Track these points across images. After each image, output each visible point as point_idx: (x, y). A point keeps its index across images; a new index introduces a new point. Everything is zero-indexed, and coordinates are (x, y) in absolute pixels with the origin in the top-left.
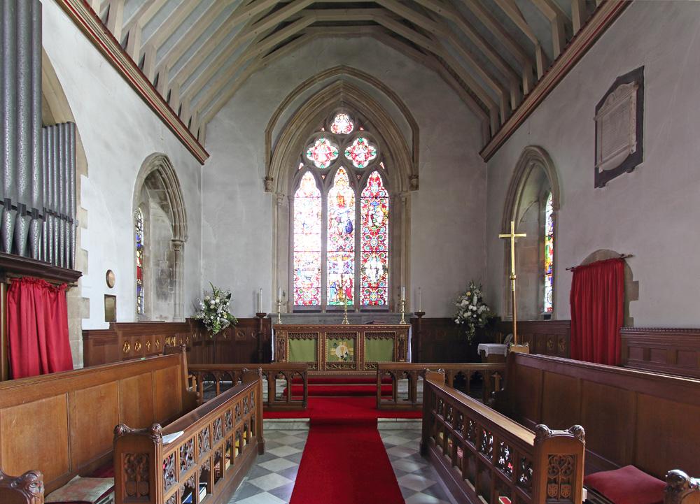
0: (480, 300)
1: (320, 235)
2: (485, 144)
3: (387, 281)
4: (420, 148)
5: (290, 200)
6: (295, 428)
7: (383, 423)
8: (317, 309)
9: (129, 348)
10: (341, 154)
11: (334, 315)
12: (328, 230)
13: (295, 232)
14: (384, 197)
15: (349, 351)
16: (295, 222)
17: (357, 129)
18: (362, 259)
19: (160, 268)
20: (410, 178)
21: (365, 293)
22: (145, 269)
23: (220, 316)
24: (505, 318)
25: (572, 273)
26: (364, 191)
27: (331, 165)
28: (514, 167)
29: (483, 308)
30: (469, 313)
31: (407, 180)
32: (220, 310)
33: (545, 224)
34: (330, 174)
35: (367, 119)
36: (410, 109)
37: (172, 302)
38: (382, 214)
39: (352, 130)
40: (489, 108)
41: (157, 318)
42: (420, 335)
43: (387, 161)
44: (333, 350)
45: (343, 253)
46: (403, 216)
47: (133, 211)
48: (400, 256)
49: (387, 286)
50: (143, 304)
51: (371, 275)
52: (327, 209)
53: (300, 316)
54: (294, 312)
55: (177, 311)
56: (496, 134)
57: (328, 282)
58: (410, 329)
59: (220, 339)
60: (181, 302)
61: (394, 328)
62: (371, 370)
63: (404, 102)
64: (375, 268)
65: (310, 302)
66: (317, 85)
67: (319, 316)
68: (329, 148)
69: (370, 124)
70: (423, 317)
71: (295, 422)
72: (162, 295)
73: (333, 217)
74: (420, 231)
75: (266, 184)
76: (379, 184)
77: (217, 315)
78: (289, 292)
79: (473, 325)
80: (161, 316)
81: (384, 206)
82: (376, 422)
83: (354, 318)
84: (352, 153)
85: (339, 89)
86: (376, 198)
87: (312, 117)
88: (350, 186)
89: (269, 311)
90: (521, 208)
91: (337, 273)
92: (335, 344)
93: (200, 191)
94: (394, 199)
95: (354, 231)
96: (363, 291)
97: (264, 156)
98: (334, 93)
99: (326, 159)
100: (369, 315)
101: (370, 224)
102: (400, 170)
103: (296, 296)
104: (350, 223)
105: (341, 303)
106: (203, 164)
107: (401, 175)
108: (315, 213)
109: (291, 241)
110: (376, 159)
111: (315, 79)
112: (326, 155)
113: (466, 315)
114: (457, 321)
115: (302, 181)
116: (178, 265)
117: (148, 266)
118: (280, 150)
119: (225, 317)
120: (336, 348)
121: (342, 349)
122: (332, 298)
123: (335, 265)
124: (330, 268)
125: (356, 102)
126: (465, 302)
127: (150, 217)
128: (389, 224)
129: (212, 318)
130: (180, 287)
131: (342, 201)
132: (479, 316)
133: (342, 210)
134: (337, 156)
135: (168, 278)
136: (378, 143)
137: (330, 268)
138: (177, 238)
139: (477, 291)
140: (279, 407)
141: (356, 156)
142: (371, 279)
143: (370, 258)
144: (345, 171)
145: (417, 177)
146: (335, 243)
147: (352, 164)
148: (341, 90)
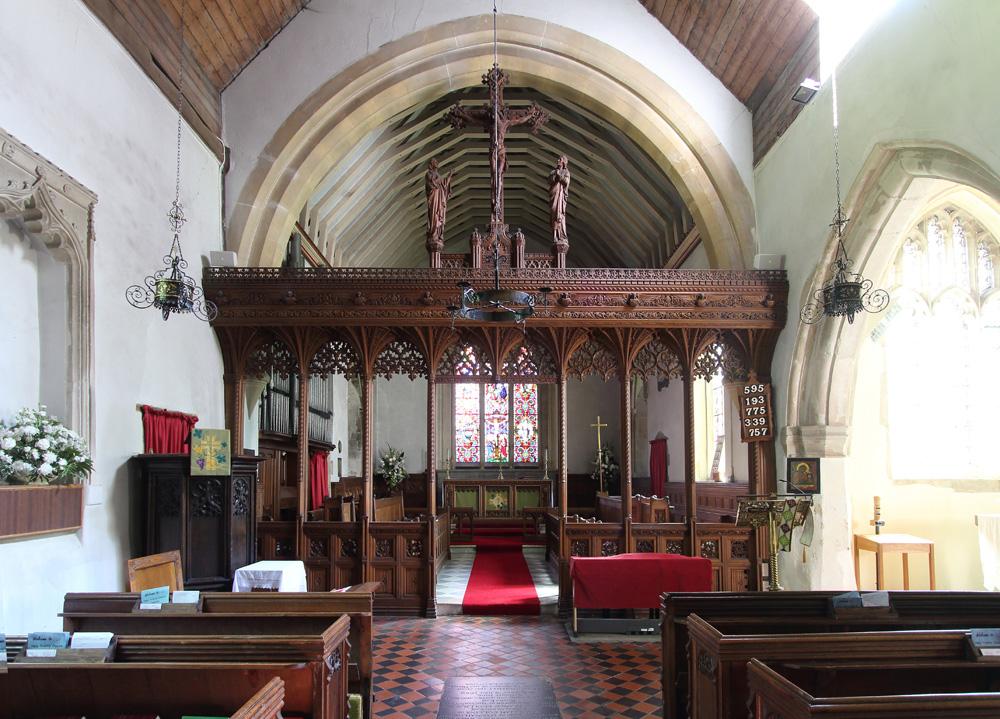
64: (527, 429)
65: (471, 459)
122: (490, 456)
123: (491, 426)
132: (611, 473)
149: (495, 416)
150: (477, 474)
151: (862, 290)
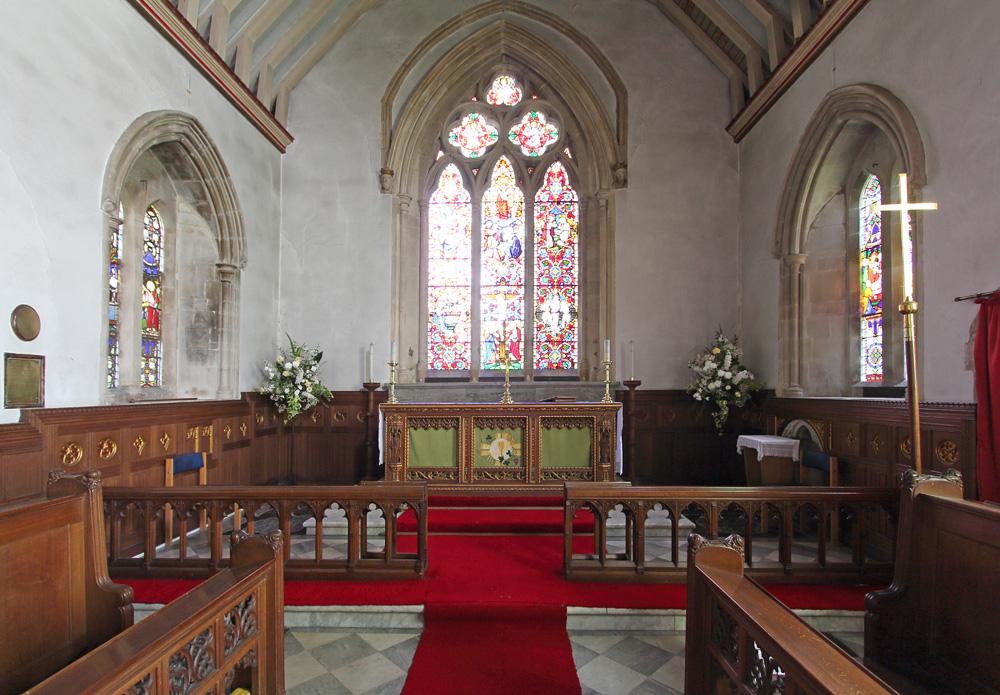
0: (735, 361)
1: (469, 261)
2: (737, 112)
3: (576, 332)
4: (629, 122)
5: (423, 206)
6: (394, 624)
7: (577, 616)
8: (465, 376)
9: (115, 450)
10: (503, 135)
11: (491, 387)
12: (482, 253)
13: (430, 256)
14: (571, 202)
15: (514, 449)
16: (430, 242)
17: (527, 97)
18: (536, 297)
19: (194, 310)
20: (614, 168)
21: (541, 350)
22: (166, 311)
23: (300, 387)
24: (784, 391)
25: (978, 306)
26: (538, 193)
27: (486, 153)
28: (802, 131)
29: (742, 375)
30: (718, 383)
31: (610, 172)
32: (299, 379)
33: (858, 229)
34: (484, 166)
35: (544, 81)
36: (611, 61)
37: (216, 366)
38: (567, 227)
39: (520, 100)
40: (746, 52)
41: (187, 392)
42: (634, 418)
43: (574, 143)
44: (485, 447)
45: (506, 289)
46: (603, 229)
47: (103, 200)
48: (598, 292)
49: (576, 339)
50: (160, 369)
51: (550, 323)
52: (480, 220)
53: (433, 388)
54: (428, 380)
55: (225, 380)
56: (756, 94)
57: (482, 333)
58: (620, 413)
59: (305, 424)
60: (232, 367)
61: (593, 410)
62: (552, 482)
63: (603, 51)
64: (557, 311)
65: (454, 365)
66: (464, 30)
67: (466, 387)
68: (483, 128)
69: (549, 90)
70: (637, 388)
71: (392, 612)
72: (196, 354)
73: (491, 232)
74: (634, 252)
75: (382, 181)
76: (563, 182)
77: (296, 386)
78: (417, 351)
79: (725, 402)
80: (195, 390)
81: (570, 215)
82: (564, 616)
83: (521, 390)
84: (520, 135)
85: (498, 33)
86: (558, 203)
87: (455, 78)
88: (517, 185)
89: (383, 377)
90: (812, 206)
91: (496, 320)
92: (489, 438)
93: (278, 194)
94: (588, 202)
95: (523, 254)
96: (538, 348)
97: (379, 137)
98: (491, 40)
99: (479, 144)
100: (547, 386)
101: (549, 243)
102: (596, 159)
103: (431, 355)
104: (518, 243)
105: (503, 367)
106: (283, 152)
107: (598, 165)
108: (462, 227)
109: (423, 269)
110: (557, 143)
111: (461, 20)
112: (480, 138)
113: (712, 386)
114: (698, 396)
115: (441, 179)
116: (227, 306)
117: (172, 307)
118: (405, 129)
119: (309, 389)
120: (490, 443)
121: (501, 445)
122: (488, 359)
123: (493, 307)
124: (486, 312)
125: (526, 54)
126: (710, 365)
127: (178, 225)
128: (579, 244)
129: (287, 391)
130: (230, 340)
131: (504, 208)
132: (735, 388)
133: (504, 222)
134: (496, 139)
135: (209, 328)
136: (560, 115)
137: (486, 312)
138: (225, 262)
139: (731, 346)
140: (369, 571)
141: (526, 139)
142: (552, 328)
143: (549, 296)
144: (508, 163)
145: (625, 166)
146: (493, 272)
147: (520, 151)
148: (502, 35)
149: (500, 288)
150: (463, 391)
151: (40, 421)
